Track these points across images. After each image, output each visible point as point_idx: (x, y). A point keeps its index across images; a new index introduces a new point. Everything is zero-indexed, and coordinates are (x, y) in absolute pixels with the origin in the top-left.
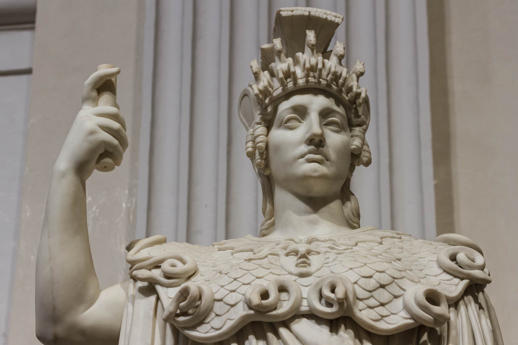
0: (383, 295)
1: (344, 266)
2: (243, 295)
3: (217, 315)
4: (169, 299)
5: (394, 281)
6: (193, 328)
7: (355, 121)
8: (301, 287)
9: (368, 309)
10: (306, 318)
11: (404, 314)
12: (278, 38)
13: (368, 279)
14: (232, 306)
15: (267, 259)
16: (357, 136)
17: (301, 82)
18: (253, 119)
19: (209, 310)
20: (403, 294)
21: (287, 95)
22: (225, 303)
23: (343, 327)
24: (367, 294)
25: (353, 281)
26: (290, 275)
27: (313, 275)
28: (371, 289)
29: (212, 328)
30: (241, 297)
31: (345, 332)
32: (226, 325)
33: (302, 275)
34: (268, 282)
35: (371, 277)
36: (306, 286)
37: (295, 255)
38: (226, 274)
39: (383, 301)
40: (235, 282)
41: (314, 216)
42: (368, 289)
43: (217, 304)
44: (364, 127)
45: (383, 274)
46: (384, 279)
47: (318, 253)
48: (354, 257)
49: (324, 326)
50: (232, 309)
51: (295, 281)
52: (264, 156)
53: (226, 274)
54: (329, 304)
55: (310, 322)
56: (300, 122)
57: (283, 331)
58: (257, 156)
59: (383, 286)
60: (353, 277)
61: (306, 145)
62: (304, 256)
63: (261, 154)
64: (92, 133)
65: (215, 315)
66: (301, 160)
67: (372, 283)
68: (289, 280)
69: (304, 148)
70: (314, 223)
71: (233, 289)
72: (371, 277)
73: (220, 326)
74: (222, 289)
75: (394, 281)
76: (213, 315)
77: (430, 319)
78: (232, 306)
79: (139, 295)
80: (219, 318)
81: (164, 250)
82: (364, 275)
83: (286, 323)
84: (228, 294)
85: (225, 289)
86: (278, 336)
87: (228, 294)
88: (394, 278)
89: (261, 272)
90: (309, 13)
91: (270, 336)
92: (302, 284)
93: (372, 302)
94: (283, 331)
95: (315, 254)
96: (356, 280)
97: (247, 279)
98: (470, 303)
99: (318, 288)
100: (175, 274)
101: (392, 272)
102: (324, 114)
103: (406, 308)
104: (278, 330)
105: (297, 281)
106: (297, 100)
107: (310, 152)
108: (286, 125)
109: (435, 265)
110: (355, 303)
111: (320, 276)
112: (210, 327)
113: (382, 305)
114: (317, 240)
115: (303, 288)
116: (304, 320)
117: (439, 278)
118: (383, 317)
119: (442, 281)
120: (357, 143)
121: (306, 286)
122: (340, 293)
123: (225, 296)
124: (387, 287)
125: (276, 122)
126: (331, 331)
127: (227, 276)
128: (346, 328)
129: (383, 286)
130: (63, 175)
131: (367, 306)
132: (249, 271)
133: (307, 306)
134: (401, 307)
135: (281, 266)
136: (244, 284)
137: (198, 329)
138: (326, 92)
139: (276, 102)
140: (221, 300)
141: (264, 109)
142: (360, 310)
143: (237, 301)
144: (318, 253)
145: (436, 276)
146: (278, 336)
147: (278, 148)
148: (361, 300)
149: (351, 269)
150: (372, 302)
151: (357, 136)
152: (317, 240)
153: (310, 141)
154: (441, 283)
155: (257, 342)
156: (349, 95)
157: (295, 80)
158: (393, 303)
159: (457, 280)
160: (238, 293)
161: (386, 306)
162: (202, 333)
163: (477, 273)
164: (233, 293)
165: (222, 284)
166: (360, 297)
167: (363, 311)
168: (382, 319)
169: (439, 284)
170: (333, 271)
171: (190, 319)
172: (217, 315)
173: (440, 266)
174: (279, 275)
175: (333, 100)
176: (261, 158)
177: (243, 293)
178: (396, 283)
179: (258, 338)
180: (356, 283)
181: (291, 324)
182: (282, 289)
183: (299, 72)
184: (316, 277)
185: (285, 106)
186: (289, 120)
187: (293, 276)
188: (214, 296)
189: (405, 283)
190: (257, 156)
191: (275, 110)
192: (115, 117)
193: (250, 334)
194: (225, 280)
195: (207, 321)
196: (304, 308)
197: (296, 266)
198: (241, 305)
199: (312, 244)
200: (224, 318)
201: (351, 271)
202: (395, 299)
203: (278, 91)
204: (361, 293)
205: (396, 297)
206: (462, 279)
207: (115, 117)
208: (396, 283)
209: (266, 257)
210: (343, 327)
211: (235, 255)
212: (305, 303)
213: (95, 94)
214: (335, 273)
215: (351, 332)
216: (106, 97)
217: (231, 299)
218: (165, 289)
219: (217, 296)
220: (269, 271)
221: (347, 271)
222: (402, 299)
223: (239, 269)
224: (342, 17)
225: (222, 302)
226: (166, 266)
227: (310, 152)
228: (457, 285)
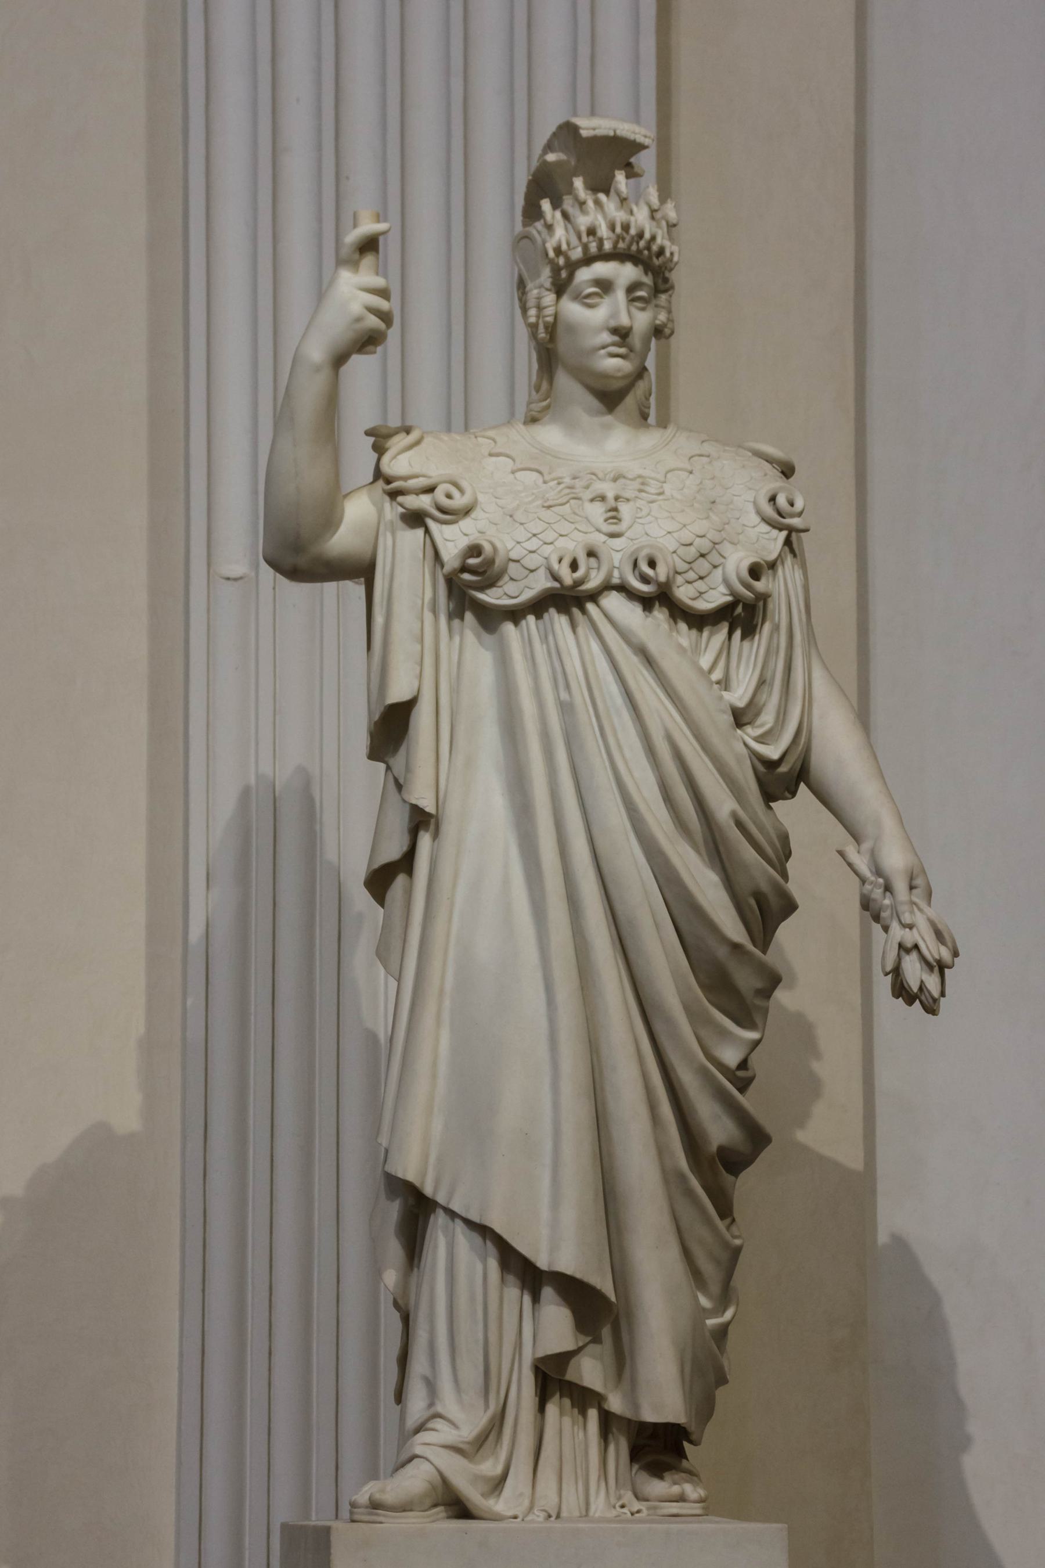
0: (703, 566)
1: (661, 527)
2: (546, 558)
3: (512, 579)
4: (445, 541)
5: (714, 547)
6: (482, 588)
7: (662, 287)
8: (612, 551)
9: (686, 584)
10: (617, 591)
11: (722, 589)
12: (579, 176)
13: (688, 547)
14: (532, 571)
15: (568, 504)
16: (663, 307)
17: (608, 246)
18: (539, 276)
19: (503, 572)
20: (722, 563)
21: (588, 260)
22: (523, 566)
23: (657, 604)
24: (686, 566)
25: (672, 551)
26: (597, 533)
27: (626, 535)
28: (691, 561)
29: (505, 594)
30: (541, 560)
31: (659, 612)
32: (523, 593)
33: (613, 535)
34: (575, 543)
35: (691, 544)
36: (617, 551)
37: (600, 501)
38: (522, 524)
39: (702, 574)
40: (534, 539)
41: (609, 418)
42: (688, 561)
43: (512, 565)
44: (670, 292)
45: (704, 538)
46: (704, 545)
47: (628, 500)
48: (670, 512)
49: (636, 604)
50: (531, 574)
51: (604, 542)
52: (550, 329)
53: (522, 524)
54: (645, 579)
55: (620, 597)
56: (602, 297)
57: (590, 607)
58: (541, 328)
59: (703, 555)
60: (670, 544)
61: (608, 333)
62: (612, 503)
63: (546, 327)
64: (359, 319)
65: (509, 578)
66: (603, 352)
67: (692, 551)
68: (598, 539)
69: (606, 337)
70: (607, 428)
71: (534, 549)
72: (691, 544)
73: (517, 594)
74: (518, 545)
75: (714, 547)
76: (506, 578)
77: (751, 597)
78: (532, 571)
79: (400, 524)
80: (515, 582)
81: (427, 458)
82: (685, 543)
83: (594, 596)
84: (526, 555)
85: (522, 546)
86: (584, 611)
87: (526, 555)
88: (715, 544)
89: (565, 527)
90: (615, 131)
91: (576, 611)
92: (613, 548)
93: (691, 575)
94: (590, 607)
95: (624, 502)
96: (675, 549)
97: (550, 536)
98: (786, 556)
99: (633, 558)
100: (455, 510)
101: (712, 535)
102: (631, 288)
103: (726, 582)
104: (585, 604)
105: (607, 542)
106: (601, 269)
107: (614, 344)
108: (585, 300)
109: (751, 508)
110: (674, 577)
111: (634, 538)
112: (502, 593)
113: (701, 578)
114: (624, 477)
115: (614, 553)
116: (614, 593)
117: (757, 529)
118: (701, 593)
119: (761, 535)
120: (662, 317)
121: (617, 551)
122: (662, 573)
123: (523, 558)
124: (707, 557)
125: (570, 289)
126: (644, 610)
127: (522, 526)
128: (660, 606)
129: (703, 555)
130: (318, 369)
131: (684, 581)
132: (551, 525)
133: (619, 578)
134: (720, 579)
135: (586, 518)
136: (545, 543)
137: (488, 591)
138: (634, 258)
139: (573, 267)
140: (518, 561)
141: (556, 270)
142: (678, 587)
143: (538, 566)
144: (628, 500)
145: (754, 527)
146: (584, 611)
147: (572, 329)
148: (680, 573)
149: (669, 533)
150: (691, 575)
151: (663, 307)
152: (624, 477)
153: (615, 331)
154: (760, 539)
155: (559, 617)
156: (660, 259)
157: (601, 241)
158: (712, 574)
159: (775, 532)
160: (539, 555)
161: (706, 580)
162: (492, 598)
163: (795, 522)
164: (532, 555)
165: (519, 540)
166: (679, 570)
167: (681, 588)
168: (700, 596)
169: (758, 540)
170: (648, 532)
171: (478, 580)
172: (512, 579)
173: (759, 512)
174: (586, 533)
175: (641, 267)
176: (546, 332)
177: (546, 556)
178: (717, 550)
179: (559, 612)
180: (674, 552)
181: (600, 598)
182: (591, 554)
183: (603, 231)
184: (628, 538)
185: (584, 275)
186: (589, 296)
187: (601, 535)
188: (508, 554)
189: (726, 548)
190: (541, 328)
191: (571, 276)
192: (383, 293)
193: (551, 606)
194: (521, 534)
195: (500, 583)
196: (616, 581)
197: (606, 520)
198: (542, 573)
199: (618, 482)
200: (522, 584)
201: (668, 535)
202: (714, 570)
203: (577, 254)
204: (681, 566)
205: (715, 567)
206: (781, 530)
207: (383, 293)
208: (717, 550)
209: (568, 502)
210: (657, 604)
211: (518, 475)
212: (616, 573)
213: (357, 256)
214: (651, 537)
215: (666, 611)
216: (368, 260)
217: (532, 561)
218: (439, 525)
219: (513, 555)
220: (573, 526)
221: (665, 535)
222: (919, 1002)
223: (537, 519)
224: (652, 137)
225: (518, 564)
226: (439, 494)
227: (614, 344)
228: (776, 539)
